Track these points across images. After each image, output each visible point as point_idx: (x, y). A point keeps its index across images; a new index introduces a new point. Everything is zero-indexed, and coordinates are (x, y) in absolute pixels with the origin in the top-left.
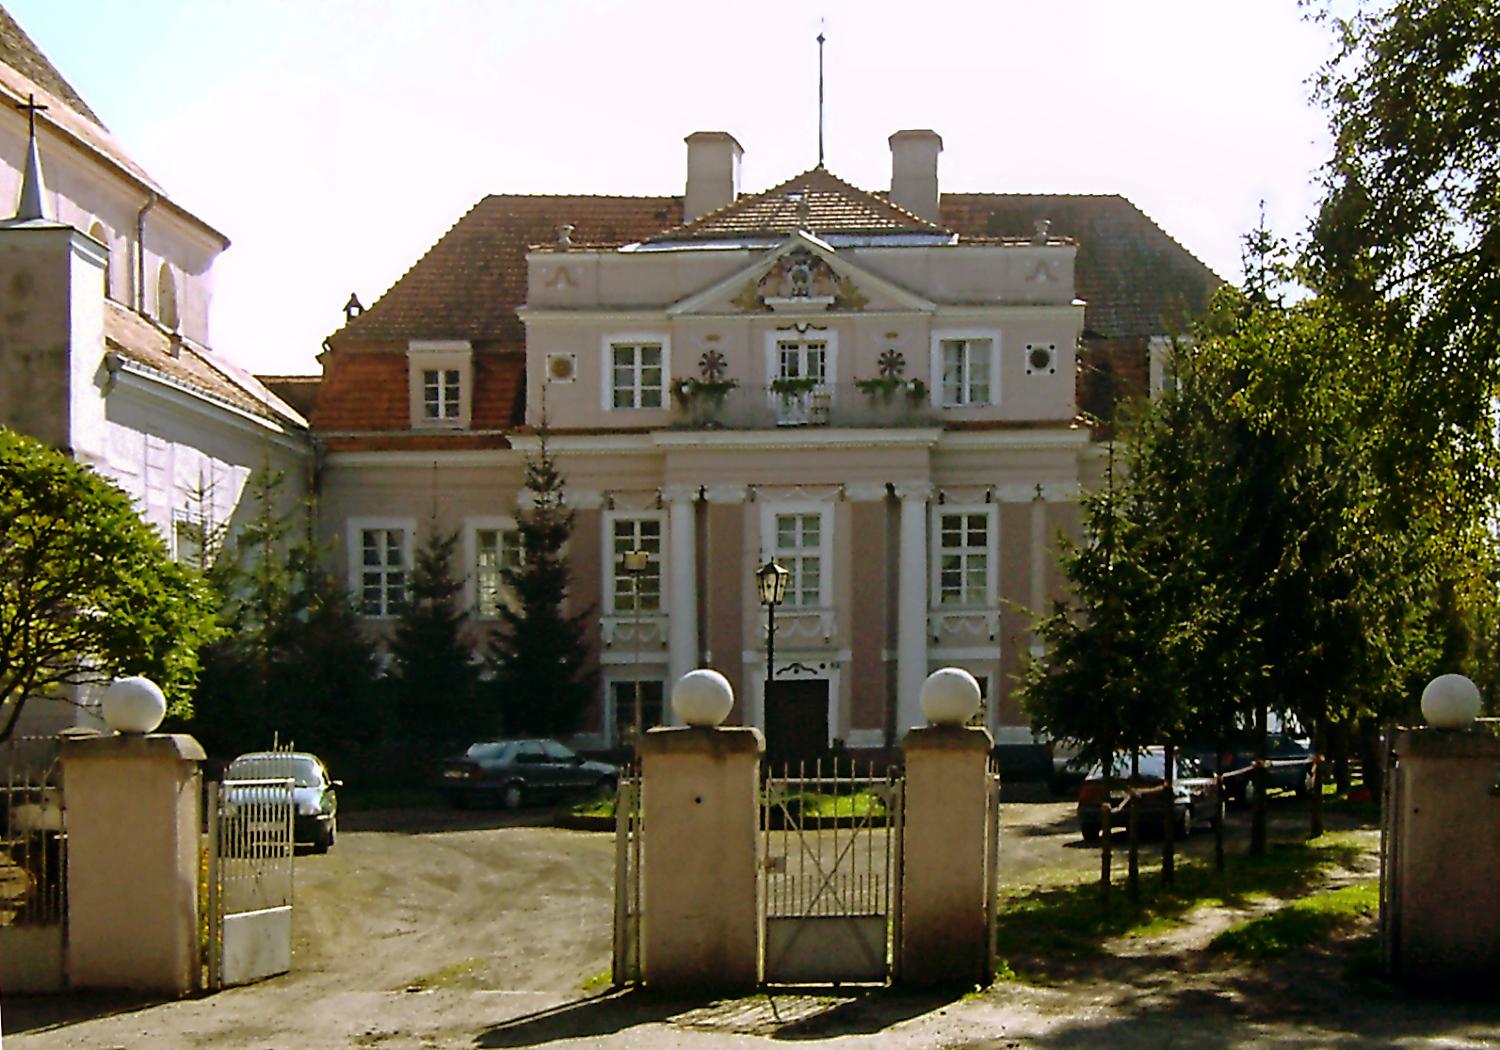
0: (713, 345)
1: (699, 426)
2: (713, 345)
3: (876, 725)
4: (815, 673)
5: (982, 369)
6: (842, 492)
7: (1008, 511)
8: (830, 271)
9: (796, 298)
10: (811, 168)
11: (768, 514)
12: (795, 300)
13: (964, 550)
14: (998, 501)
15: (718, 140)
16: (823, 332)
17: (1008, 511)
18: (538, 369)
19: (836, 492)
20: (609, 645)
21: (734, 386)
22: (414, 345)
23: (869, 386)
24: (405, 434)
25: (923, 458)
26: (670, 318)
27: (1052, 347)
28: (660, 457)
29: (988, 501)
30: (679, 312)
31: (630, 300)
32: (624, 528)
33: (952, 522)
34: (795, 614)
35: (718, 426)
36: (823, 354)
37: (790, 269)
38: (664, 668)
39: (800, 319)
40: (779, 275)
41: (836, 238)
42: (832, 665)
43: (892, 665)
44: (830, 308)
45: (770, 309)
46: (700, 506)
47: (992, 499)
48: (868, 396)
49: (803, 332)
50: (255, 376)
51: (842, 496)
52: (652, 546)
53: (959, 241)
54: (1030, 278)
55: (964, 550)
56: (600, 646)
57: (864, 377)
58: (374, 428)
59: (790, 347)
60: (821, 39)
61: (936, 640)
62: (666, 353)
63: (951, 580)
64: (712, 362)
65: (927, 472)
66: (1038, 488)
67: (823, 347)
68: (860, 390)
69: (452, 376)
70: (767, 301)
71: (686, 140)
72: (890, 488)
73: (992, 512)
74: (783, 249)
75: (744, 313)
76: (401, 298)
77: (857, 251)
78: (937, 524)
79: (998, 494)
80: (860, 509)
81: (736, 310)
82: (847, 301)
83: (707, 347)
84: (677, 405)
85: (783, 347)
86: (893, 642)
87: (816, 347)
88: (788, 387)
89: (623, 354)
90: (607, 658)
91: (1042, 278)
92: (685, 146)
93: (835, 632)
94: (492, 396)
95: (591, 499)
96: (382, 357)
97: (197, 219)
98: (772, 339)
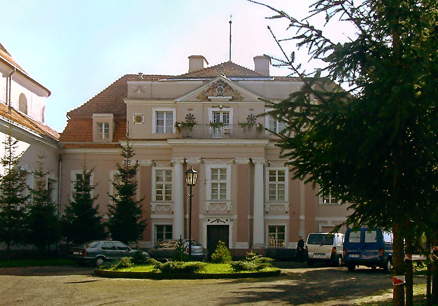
0: (191, 112)
1: (184, 138)
2: (191, 112)
4: (225, 222)
6: (234, 161)
8: (231, 88)
9: (219, 97)
10: (227, 61)
13: (277, 182)
15: (201, 58)
16: (229, 108)
18: (131, 117)
21: (196, 124)
22: (94, 115)
23: (243, 125)
24: (90, 143)
25: (262, 150)
26: (176, 102)
28: (170, 149)
30: (179, 101)
31: (162, 97)
33: (272, 173)
34: (218, 202)
35: (190, 138)
36: (228, 116)
37: (217, 87)
38: (172, 220)
39: (220, 104)
40: (213, 89)
41: (233, 78)
43: (252, 220)
44: (230, 100)
45: (210, 100)
48: (243, 128)
49: (221, 108)
50: (59, 133)
52: (170, 179)
53: (275, 79)
55: (277, 182)
56: (150, 212)
57: (241, 122)
58: (81, 141)
59: (217, 114)
60: (230, 22)
61: (267, 213)
62: (174, 113)
63: (273, 192)
64: (190, 117)
65: (264, 155)
67: (228, 114)
68: (240, 126)
69: (107, 125)
70: (209, 98)
71: (188, 57)
72: (251, 160)
74: (215, 81)
75: (201, 101)
76: (94, 102)
77: (240, 82)
78: (267, 173)
80: (240, 167)
82: (237, 98)
83: (188, 113)
84: (178, 132)
85: (215, 114)
86: (252, 213)
88: (216, 125)
90: (153, 216)
92: (188, 60)
93: (231, 208)
94: (120, 132)
95: (145, 162)
96: (85, 120)
97: (35, 81)
98: (211, 110)
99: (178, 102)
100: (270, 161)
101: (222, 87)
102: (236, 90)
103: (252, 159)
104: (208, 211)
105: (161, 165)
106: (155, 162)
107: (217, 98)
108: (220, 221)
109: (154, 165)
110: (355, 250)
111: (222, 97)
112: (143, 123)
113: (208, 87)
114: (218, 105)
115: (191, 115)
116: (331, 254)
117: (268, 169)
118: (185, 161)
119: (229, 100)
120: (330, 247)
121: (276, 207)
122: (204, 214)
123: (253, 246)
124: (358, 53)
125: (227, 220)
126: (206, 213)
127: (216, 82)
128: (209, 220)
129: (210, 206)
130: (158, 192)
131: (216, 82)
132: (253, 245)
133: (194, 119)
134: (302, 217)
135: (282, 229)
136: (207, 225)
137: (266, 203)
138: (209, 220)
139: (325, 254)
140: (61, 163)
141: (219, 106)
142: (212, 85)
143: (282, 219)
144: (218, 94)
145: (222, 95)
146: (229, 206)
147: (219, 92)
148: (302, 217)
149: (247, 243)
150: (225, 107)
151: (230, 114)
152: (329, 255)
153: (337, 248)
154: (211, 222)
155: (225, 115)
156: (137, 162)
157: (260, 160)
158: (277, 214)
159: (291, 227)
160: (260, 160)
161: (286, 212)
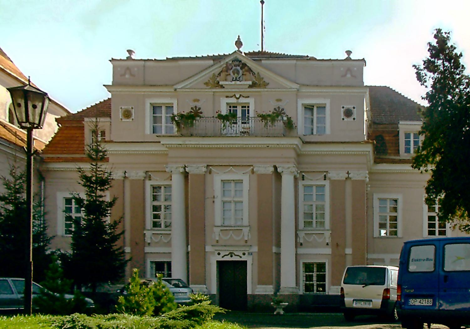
0: (196, 104)
2: (196, 104)
3: (271, 284)
4: (241, 257)
5: (322, 120)
7: (334, 183)
8: (250, 70)
11: (217, 178)
12: (233, 82)
14: (330, 179)
16: (249, 98)
17: (334, 183)
19: (250, 169)
20: (149, 243)
25: (292, 154)
27: (132, 108)
29: (325, 179)
30: (180, 87)
32: (156, 188)
36: (248, 110)
40: (227, 71)
42: (249, 254)
43: (278, 255)
44: (250, 86)
45: (222, 87)
46: (186, 175)
47: (326, 178)
51: (253, 172)
54: (345, 76)
59: (234, 107)
61: (301, 244)
66: (348, 173)
67: (248, 107)
69: (321, 266)
70: (221, 83)
72: (276, 168)
73: (327, 183)
79: (329, 175)
80: (261, 177)
81: (206, 87)
82: (258, 83)
83: (193, 105)
85: (230, 107)
86: (278, 245)
87: (245, 107)
89: (155, 108)
90: (147, 249)
91: (349, 76)
93: (250, 237)
99: (179, 89)
100: (303, 172)
101: (239, 68)
102: (258, 73)
103: (277, 166)
104: (217, 241)
105: (158, 179)
106: (150, 174)
107: (232, 83)
108: (234, 254)
109: (148, 179)
110: (164, 266)
111: (238, 82)
112: (133, 119)
113: (220, 69)
114: (234, 94)
115: (197, 109)
116: (381, 300)
117: (301, 183)
118: (185, 169)
119: (249, 87)
120: (379, 289)
121: (312, 237)
122: (212, 246)
123: (280, 291)
124: (429, 99)
125: (244, 254)
126: (215, 243)
127: (230, 61)
128: (219, 254)
129: (220, 234)
130: (156, 217)
131: (231, 62)
132: (280, 288)
133: (201, 113)
134: (349, 251)
135: (321, 266)
136: (217, 261)
137: (300, 230)
138: (219, 254)
139: (371, 301)
140: (43, 183)
141: (235, 95)
142: (225, 66)
143: (320, 253)
144: (233, 78)
145: (238, 79)
146: (246, 234)
147: (234, 75)
148: (349, 251)
149: (271, 286)
150: (243, 97)
151: (250, 107)
152: (377, 303)
153: (390, 289)
154: (223, 257)
155: (245, 109)
156: (125, 174)
157: (288, 168)
158: (315, 246)
159: (333, 265)
160: (288, 168)
161: (327, 244)
